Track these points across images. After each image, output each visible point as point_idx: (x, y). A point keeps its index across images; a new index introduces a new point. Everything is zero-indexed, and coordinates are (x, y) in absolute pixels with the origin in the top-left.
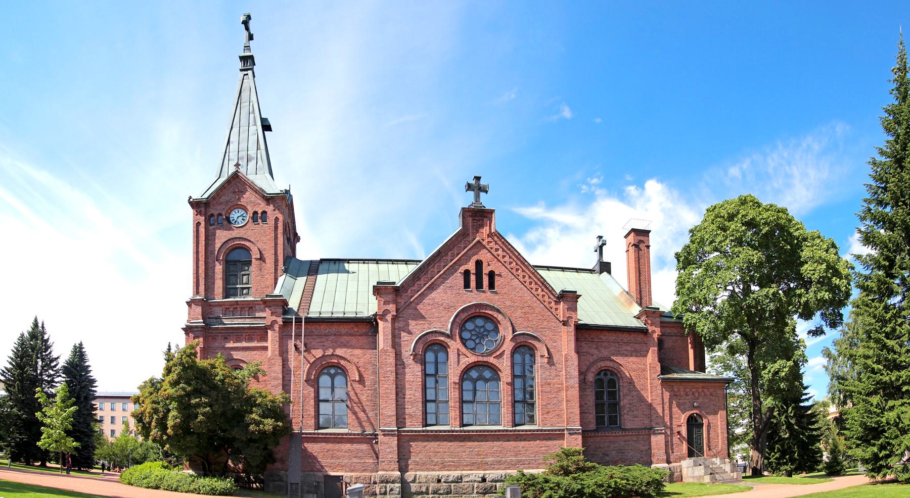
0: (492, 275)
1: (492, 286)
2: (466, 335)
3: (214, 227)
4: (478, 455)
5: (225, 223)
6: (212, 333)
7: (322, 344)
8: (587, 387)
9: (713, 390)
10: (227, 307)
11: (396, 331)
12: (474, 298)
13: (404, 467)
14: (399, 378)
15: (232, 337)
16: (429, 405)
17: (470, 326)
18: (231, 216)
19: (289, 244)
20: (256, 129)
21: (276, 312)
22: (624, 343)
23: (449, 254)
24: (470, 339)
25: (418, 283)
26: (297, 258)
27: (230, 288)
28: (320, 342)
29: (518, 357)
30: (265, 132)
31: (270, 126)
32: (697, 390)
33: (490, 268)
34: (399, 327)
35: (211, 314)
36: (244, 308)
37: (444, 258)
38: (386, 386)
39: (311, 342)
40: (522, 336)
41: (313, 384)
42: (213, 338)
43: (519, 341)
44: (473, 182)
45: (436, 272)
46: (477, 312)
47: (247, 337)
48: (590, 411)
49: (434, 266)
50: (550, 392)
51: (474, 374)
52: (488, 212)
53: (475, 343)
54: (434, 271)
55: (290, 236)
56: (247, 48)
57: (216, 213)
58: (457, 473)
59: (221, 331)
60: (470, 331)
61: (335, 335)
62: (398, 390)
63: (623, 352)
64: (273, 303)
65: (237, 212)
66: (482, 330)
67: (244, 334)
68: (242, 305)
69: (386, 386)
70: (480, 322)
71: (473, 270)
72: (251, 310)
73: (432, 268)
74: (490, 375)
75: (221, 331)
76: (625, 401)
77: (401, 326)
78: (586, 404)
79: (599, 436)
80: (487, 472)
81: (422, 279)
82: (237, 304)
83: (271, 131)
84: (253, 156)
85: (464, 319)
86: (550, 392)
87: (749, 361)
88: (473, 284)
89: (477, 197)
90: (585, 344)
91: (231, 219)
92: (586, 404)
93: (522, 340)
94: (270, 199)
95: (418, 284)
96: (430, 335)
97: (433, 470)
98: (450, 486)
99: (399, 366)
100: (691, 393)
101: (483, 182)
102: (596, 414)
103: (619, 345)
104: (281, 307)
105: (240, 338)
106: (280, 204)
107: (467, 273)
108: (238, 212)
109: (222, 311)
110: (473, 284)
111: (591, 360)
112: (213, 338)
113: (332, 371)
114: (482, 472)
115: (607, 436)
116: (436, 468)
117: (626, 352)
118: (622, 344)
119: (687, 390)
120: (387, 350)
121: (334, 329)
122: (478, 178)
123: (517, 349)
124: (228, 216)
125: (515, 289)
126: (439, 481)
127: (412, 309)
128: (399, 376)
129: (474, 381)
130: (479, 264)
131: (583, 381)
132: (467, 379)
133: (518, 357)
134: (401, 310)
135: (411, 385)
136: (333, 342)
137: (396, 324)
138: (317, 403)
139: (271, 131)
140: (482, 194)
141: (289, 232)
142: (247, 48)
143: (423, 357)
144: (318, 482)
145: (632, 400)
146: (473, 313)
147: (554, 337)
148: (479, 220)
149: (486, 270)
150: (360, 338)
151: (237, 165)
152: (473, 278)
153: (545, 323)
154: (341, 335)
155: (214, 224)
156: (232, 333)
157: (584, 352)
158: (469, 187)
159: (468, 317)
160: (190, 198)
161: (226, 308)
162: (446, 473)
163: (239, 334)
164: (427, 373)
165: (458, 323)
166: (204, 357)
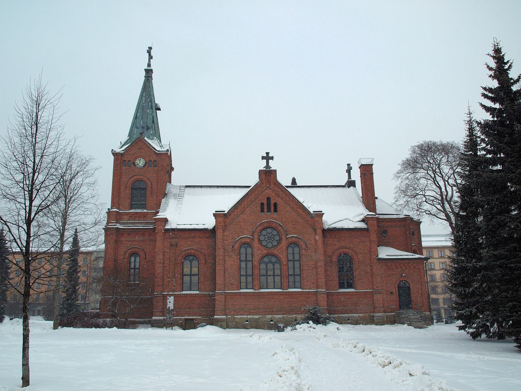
0: (275, 205)
1: (275, 210)
2: (262, 238)
4: (268, 306)
5: (132, 165)
7: (186, 243)
8: (333, 265)
9: (416, 265)
13: (228, 313)
16: (242, 277)
17: (264, 232)
25: (237, 210)
29: (290, 250)
33: (274, 202)
44: (265, 155)
48: (334, 279)
49: (244, 202)
51: (266, 259)
53: (271, 242)
54: (245, 204)
56: (149, 65)
57: (127, 160)
63: (354, 243)
65: (143, 162)
70: (269, 230)
71: (265, 202)
74: (275, 260)
76: (356, 273)
82: (137, 214)
83: (160, 110)
86: (308, 269)
87: (23, 321)
88: (266, 210)
89: (268, 163)
90: (331, 239)
99: (226, 257)
100: (400, 267)
101: (270, 155)
102: (339, 281)
107: (262, 204)
108: (143, 163)
110: (266, 210)
118: (354, 238)
119: (397, 265)
122: (268, 154)
123: (290, 245)
124: (134, 162)
125: (288, 212)
129: (267, 264)
130: (268, 199)
131: (330, 261)
132: (262, 263)
133: (290, 250)
138: (182, 276)
139: (160, 110)
140: (270, 161)
142: (149, 65)
143: (239, 251)
147: (310, 237)
149: (272, 202)
152: (265, 207)
158: (263, 158)
159: (263, 228)
160: (113, 150)
161: (130, 216)
164: (241, 260)
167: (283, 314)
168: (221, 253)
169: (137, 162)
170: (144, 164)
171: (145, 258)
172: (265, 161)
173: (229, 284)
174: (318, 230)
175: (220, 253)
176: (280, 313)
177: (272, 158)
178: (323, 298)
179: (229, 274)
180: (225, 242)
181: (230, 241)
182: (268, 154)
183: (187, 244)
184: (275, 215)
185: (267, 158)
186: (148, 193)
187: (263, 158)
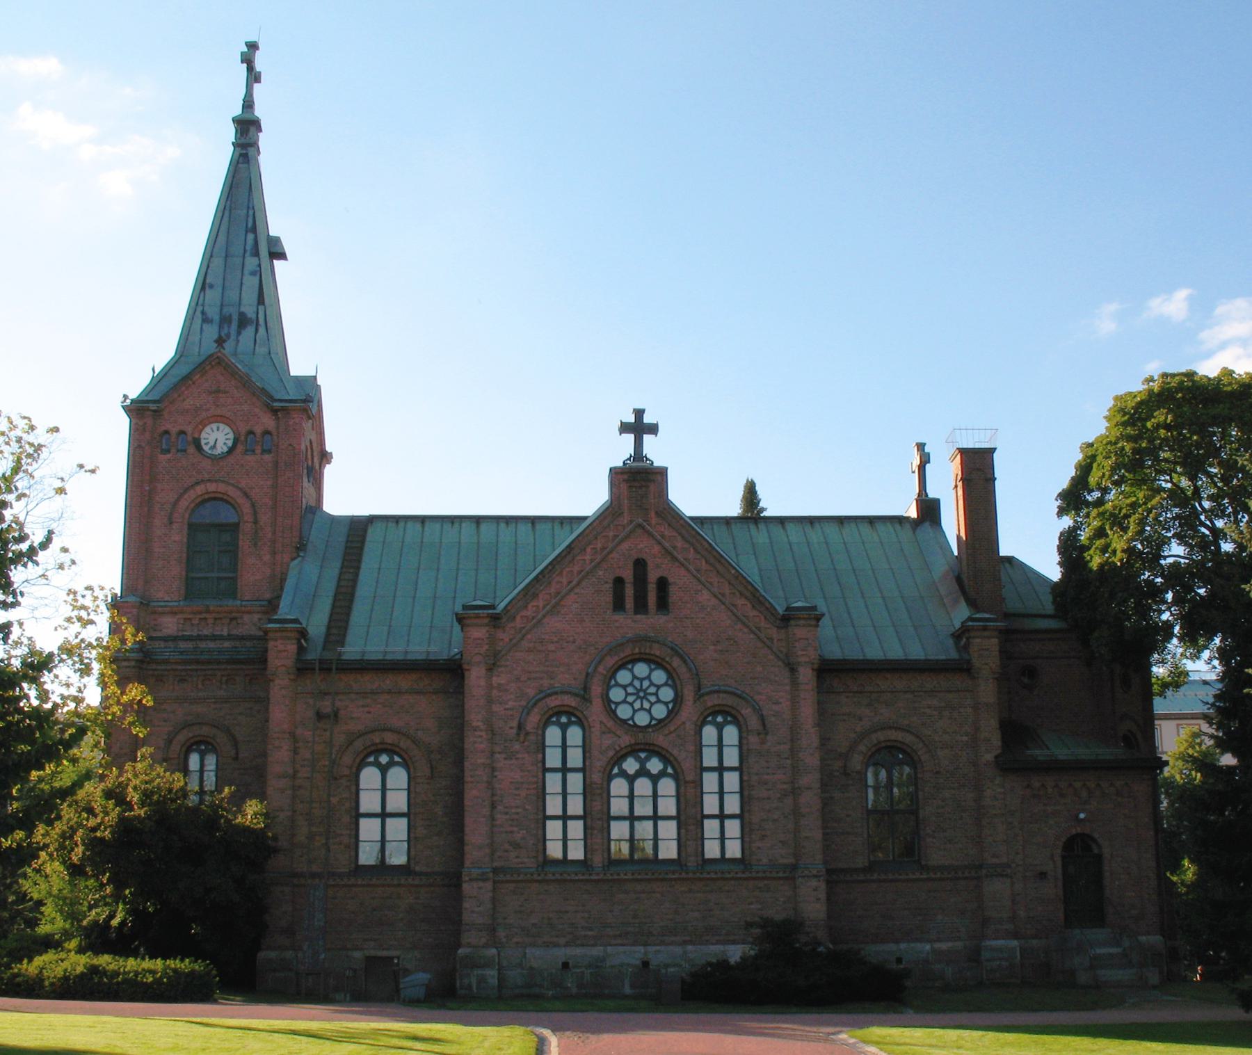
0: (663, 584)
1: (663, 604)
3: (169, 456)
6: (155, 670)
7: (367, 709)
8: (851, 782)
10: (189, 617)
11: (495, 692)
12: (629, 624)
14: (499, 777)
15: (195, 679)
18: (203, 435)
19: (311, 479)
20: (257, 262)
21: (287, 651)
22: (926, 692)
23: (588, 550)
24: (624, 701)
25: (533, 603)
26: (324, 509)
27: (192, 578)
28: (363, 706)
30: (275, 261)
31: (285, 254)
32: (1084, 785)
34: (499, 684)
35: (155, 630)
36: (221, 619)
37: (579, 558)
38: (475, 792)
39: (347, 707)
40: (716, 695)
41: (348, 784)
42: (157, 680)
43: (709, 704)
44: (631, 419)
45: (565, 583)
46: (636, 654)
47: (224, 679)
49: (561, 573)
50: (769, 798)
52: (657, 473)
55: (313, 462)
56: (248, 104)
58: (597, 951)
59: (174, 667)
60: (624, 687)
61: (389, 692)
62: (495, 798)
64: (279, 634)
65: (215, 429)
66: (646, 684)
67: (219, 673)
68: (218, 612)
69: (475, 792)
71: (628, 575)
72: (234, 622)
73: (557, 575)
75: (174, 667)
77: (502, 682)
78: (848, 816)
79: (873, 881)
80: (651, 949)
81: (541, 596)
84: (249, 316)
85: (612, 667)
86: (769, 798)
88: (629, 603)
89: (639, 444)
91: (203, 442)
92: (848, 816)
93: (716, 703)
94: (279, 410)
95: (533, 606)
96: (553, 698)
97: (556, 945)
98: (583, 973)
101: (647, 419)
103: (915, 696)
104: (295, 641)
105: (209, 680)
106: (297, 420)
107: (619, 582)
108: (218, 430)
109: (179, 623)
110: (629, 603)
111: (858, 729)
112: (157, 680)
113: (384, 759)
114: (642, 949)
115: (892, 881)
116: (562, 941)
117: (928, 711)
120: (478, 727)
121: (388, 681)
124: (196, 436)
126: (565, 965)
127: (522, 651)
128: (496, 774)
130: (640, 565)
134: (503, 653)
135: (517, 789)
136: (385, 706)
137: (494, 678)
140: (647, 439)
141: (312, 455)
142: (248, 104)
143: (540, 738)
144: (355, 971)
145: (943, 807)
146: (629, 655)
148: (640, 487)
149: (653, 576)
150: (434, 697)
151: (220, 341)
152: (629, 591)
153: (759, 668)
154: (399, 693)
155: (168, 451)
156: (197, 670)
157: (844, 715)
158: (625, 428)
160: (125, 397)
162: (578, 951)
163: (210, 672)
165: (603, 674)
166: (228, 803)
167: (685, 943)
168: (481, 743)
169: (206, 436)
170: (230, 443)
171: (236, 758)
172: (630, 438)
173: (507, 846)
174: (801, 670)
175: (476, 745)
176: (673, 939)
177: (653, 429)
178: (815, 890)
179: (507, 813)
180: (496, 708)
181: (511, 704)
182: (639, 413)
183: (369, 712)
184: (661, 620)
185: (639, 428)
186: (244, 542)
187: (625, 428)
